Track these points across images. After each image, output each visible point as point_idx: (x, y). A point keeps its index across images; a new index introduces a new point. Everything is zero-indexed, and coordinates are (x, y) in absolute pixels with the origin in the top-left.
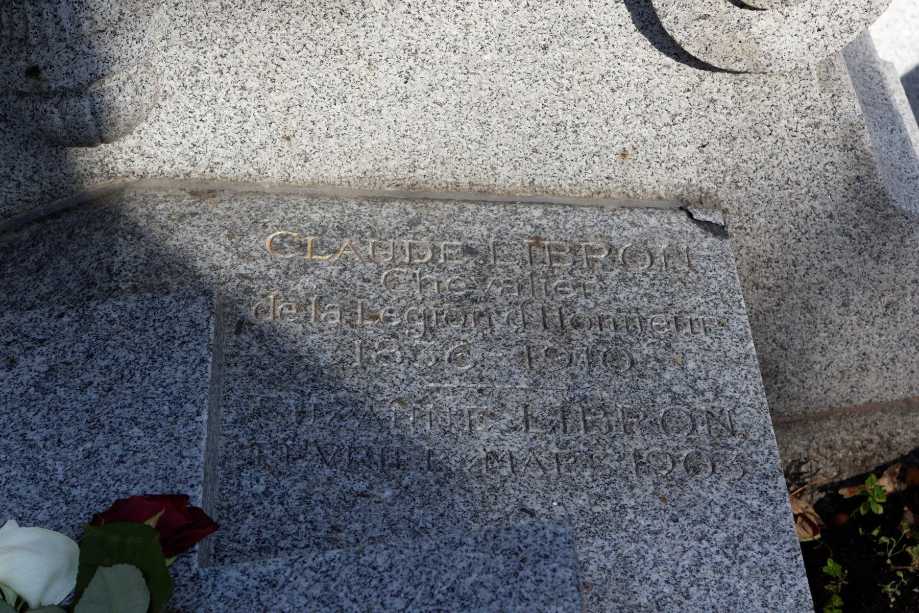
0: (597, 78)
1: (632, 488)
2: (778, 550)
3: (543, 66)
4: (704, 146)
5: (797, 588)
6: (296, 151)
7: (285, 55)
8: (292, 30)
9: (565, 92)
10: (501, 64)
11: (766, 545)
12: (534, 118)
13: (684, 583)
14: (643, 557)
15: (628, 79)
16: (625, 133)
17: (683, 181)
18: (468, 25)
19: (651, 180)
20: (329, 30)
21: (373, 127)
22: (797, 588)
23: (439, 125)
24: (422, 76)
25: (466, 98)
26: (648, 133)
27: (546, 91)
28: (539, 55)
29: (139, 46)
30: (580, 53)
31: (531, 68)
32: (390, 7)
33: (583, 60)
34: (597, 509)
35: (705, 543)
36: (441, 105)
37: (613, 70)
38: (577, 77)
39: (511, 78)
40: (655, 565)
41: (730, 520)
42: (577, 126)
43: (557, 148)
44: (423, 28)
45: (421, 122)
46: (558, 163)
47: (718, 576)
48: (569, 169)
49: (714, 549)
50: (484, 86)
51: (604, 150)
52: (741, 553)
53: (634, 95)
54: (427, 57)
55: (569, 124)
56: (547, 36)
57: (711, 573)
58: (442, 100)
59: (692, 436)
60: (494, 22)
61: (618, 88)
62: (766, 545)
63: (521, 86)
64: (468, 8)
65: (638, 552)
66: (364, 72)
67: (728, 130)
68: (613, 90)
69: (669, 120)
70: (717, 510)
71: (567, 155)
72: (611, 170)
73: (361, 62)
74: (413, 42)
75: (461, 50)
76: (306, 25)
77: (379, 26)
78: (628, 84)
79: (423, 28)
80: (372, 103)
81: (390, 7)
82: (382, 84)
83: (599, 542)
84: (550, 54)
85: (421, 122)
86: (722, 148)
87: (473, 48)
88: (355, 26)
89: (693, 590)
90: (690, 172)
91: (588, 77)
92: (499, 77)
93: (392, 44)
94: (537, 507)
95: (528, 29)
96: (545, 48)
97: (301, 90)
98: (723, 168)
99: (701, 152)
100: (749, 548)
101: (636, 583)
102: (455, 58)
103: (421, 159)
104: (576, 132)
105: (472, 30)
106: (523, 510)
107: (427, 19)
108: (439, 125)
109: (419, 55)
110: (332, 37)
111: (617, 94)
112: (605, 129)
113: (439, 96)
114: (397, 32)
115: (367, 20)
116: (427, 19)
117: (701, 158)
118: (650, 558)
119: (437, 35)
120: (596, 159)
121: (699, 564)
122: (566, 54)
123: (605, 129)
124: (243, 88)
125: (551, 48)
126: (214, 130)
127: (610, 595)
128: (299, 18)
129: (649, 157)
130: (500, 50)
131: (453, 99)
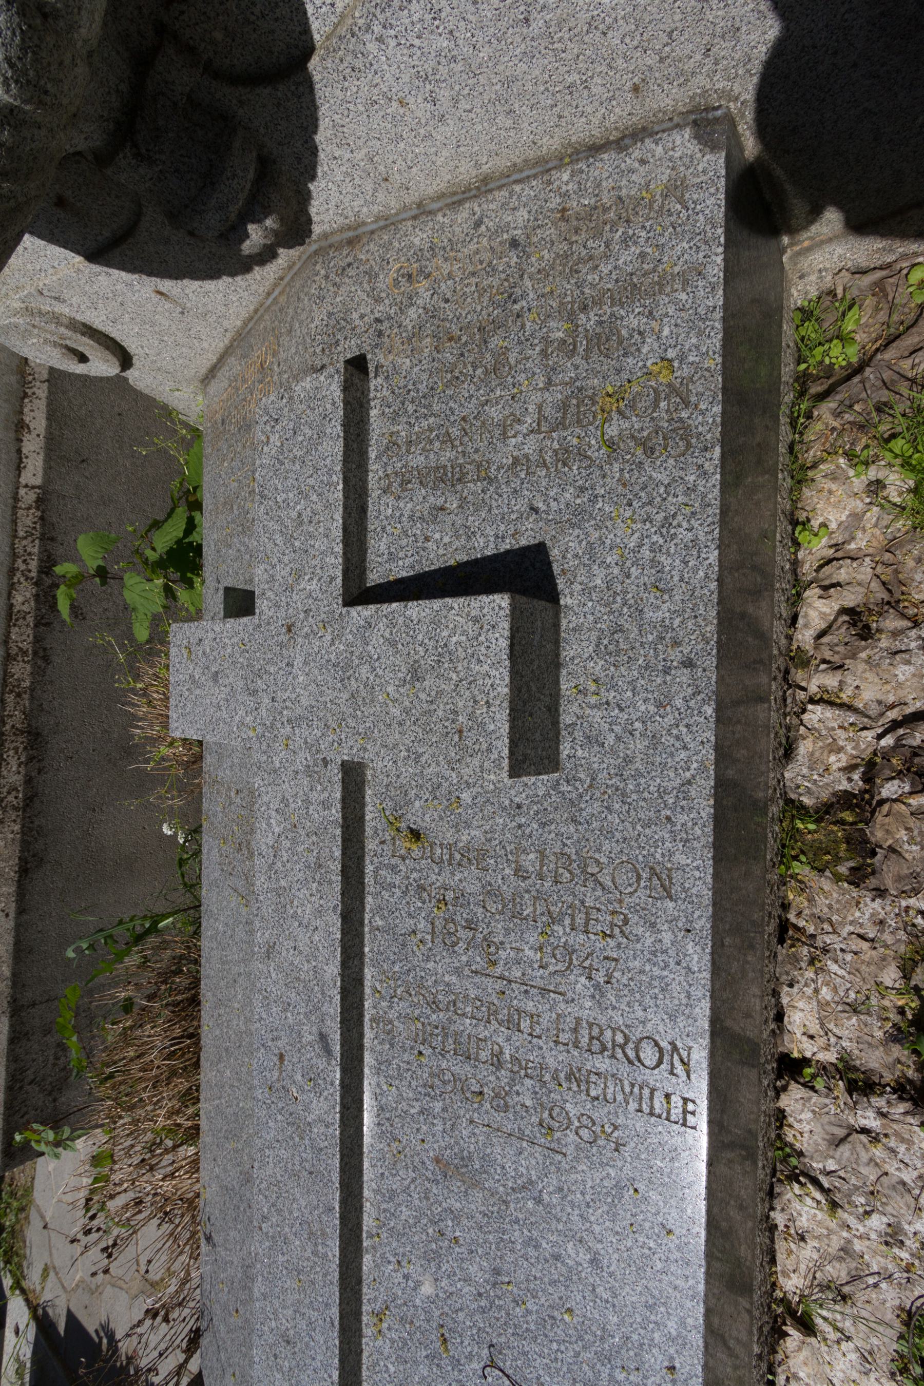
0: (585, 29)
1: (604, 477)
2: (701, 525)
3: (533, 39)
4: (709, 50)
5: (708, 562)
6: (397, 186)
7: (341, 122)
8: (332, 101)
9: (563, 55)
10: (497, 55)
11: (693, 521)
12: (547, 89)
13: (628, 564)
14: (604, 543)
15: (614, 15)
16: (631, 69)
17: (698, 91)
18: (451, 32)
19: (668, 101)
20: (355, 89)
21: (434, 149)
22: (708, 562)
23: (479, 127)
24: (444, 94)
25: (486, 97)
26: (651, 60)
27: (546, 61)
28: (525, 30)
29: (235, 181)
30: (559, 11)
31: (523, 46)
32: (383, 47)
33: (565, 16)
34: (578, 501)
35: (648, 525)
36: (470, 111)
37: (595, 13)
38: (567, 36)
39: (511, 64)
40: (611, 549)
41: (670, 499)
42: (586, 81)
43: (577, 107)
44: (419, 53)
45: (464, 131)
46: (584, 120)
47: (652, 555)
48: (594, 120)
49: (653, 530)
50: (494, 81)
51: (617, 93)
52: (673, 531)
53: (625, 28)
54: (438, 77)
55: (578, 82)
56: (522, 8)
57: (648, 552)
58: (468, 107)
59: (655, 415)
60: (471, 18)
61: (609, 28)
62: (693, 521)
63: (523, 67)
64: (443, 15)
65: (600, 539)
66: (401, 111)
67: (729, 24)
68: (605, 34)
69: (666, 39)
70: (662, 490)
71: (589, 109)
72: (630, 107)
73: (394, 104)
74: (420, 69)
75: (460, 58)
76: (338, 93)
77: (386, 67)
78: (616, 20)
79: (419, 53)
80: (422, 131)
81: (383, 47)
82: (419, 114)
83: (577, 531)
84: (534, 25)
85: (464, 131)
86: (727, 44)
87: (467, 50)
88: (370, 76)
89: (633, 569)
90: (701, 80)
91: (576, 31)
92: (501, 68)
93: (406, 78)
94: (540, 505)
95: (503, 10)
96: (527, 20)
97: (369, 143)
98: (734, 63)
99: (709, 56)
100: (679, 526)
101: (596, 567)
102: (459, 67)
103: (479, 157)
104: (586, 87)
105: (458, 35)
106: (532, 509)
107: (417, 42)
108: (479, 127)
109: (431, 78)
110: (360, 93)
111: (610, 35)
112: (611, 74)
113: (464, 105)
114: (402, 66)
115: (375, 67)
116: (417, 42)
117: (709, 62)
118: (608, 541)
119: (433, 54)
120: (614, 103)
121: (641, 546)
122: (548, 18)
123: (611, 74)
124: (335, 158)
125: (531, 18)
126: (341, 193)
127: (579, 579)
128: (329, 89)
129: (659, 81)
130: (489, 42)
131: (477, 102)
